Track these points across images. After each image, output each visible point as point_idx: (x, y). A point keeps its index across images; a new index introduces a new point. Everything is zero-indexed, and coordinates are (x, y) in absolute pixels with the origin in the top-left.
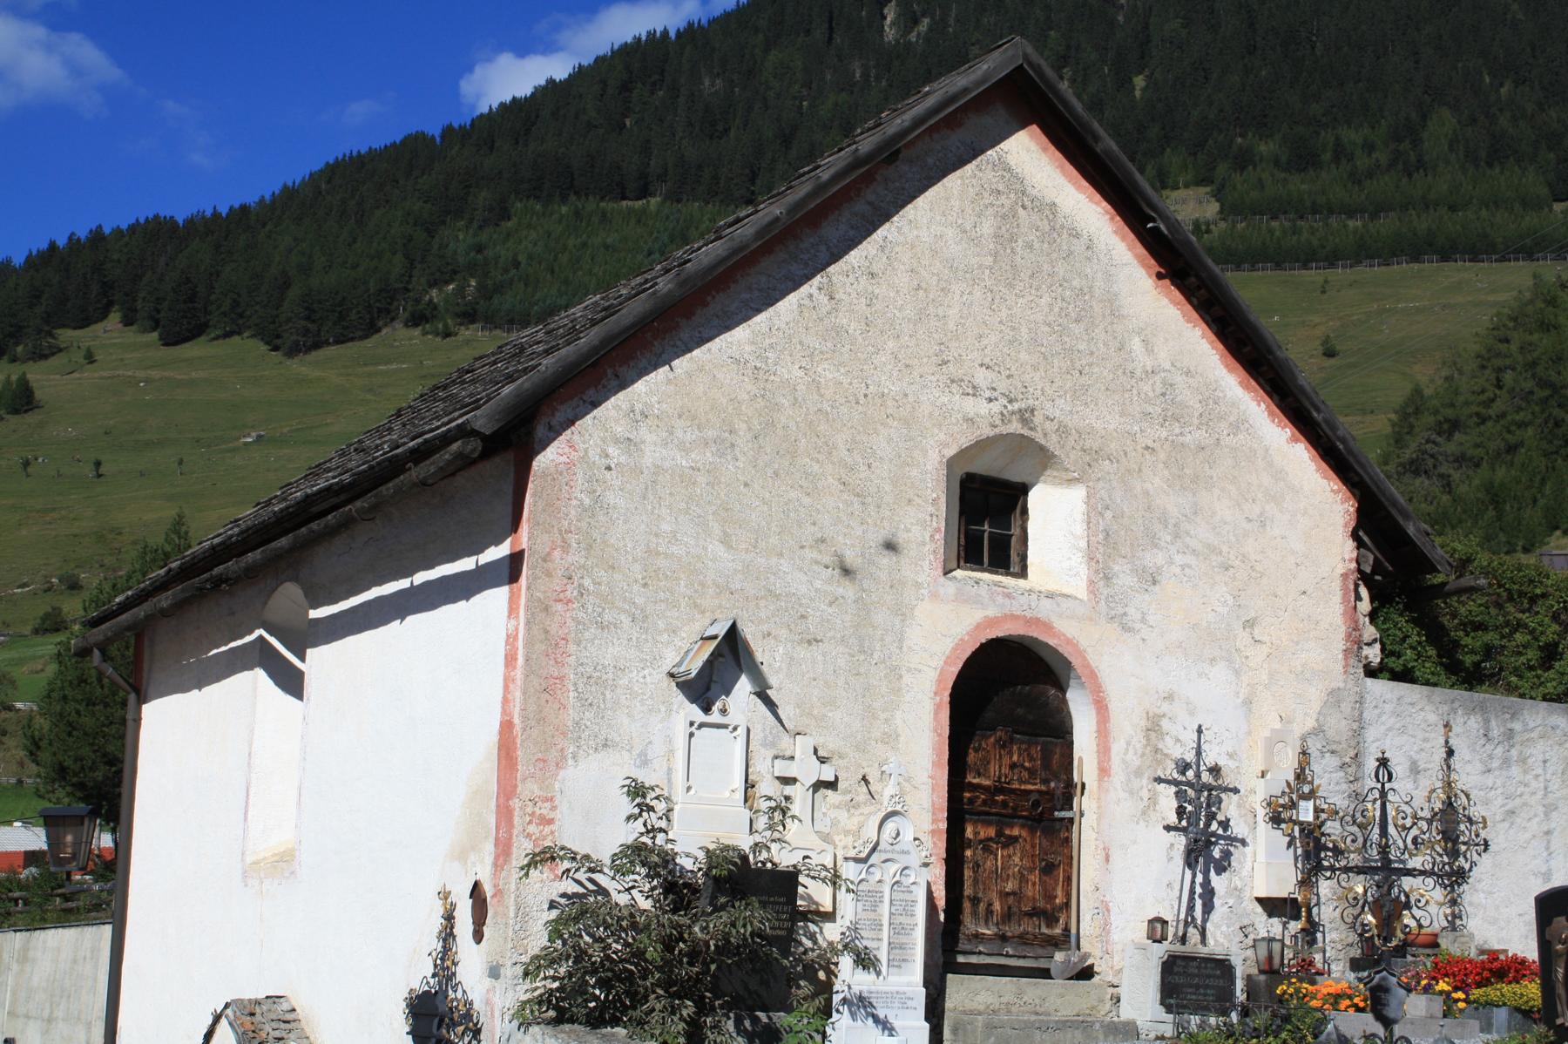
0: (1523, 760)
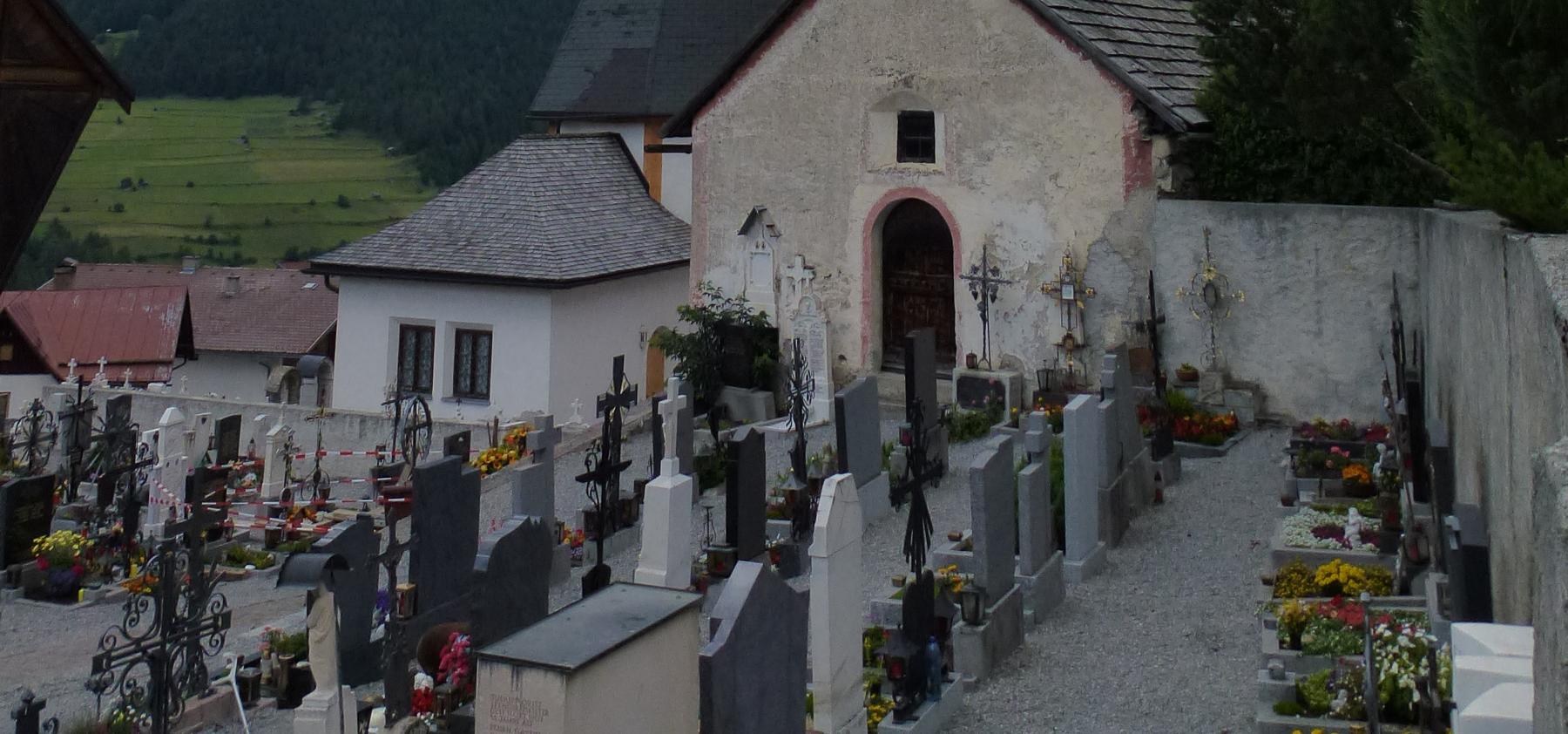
0: (1295, 250)
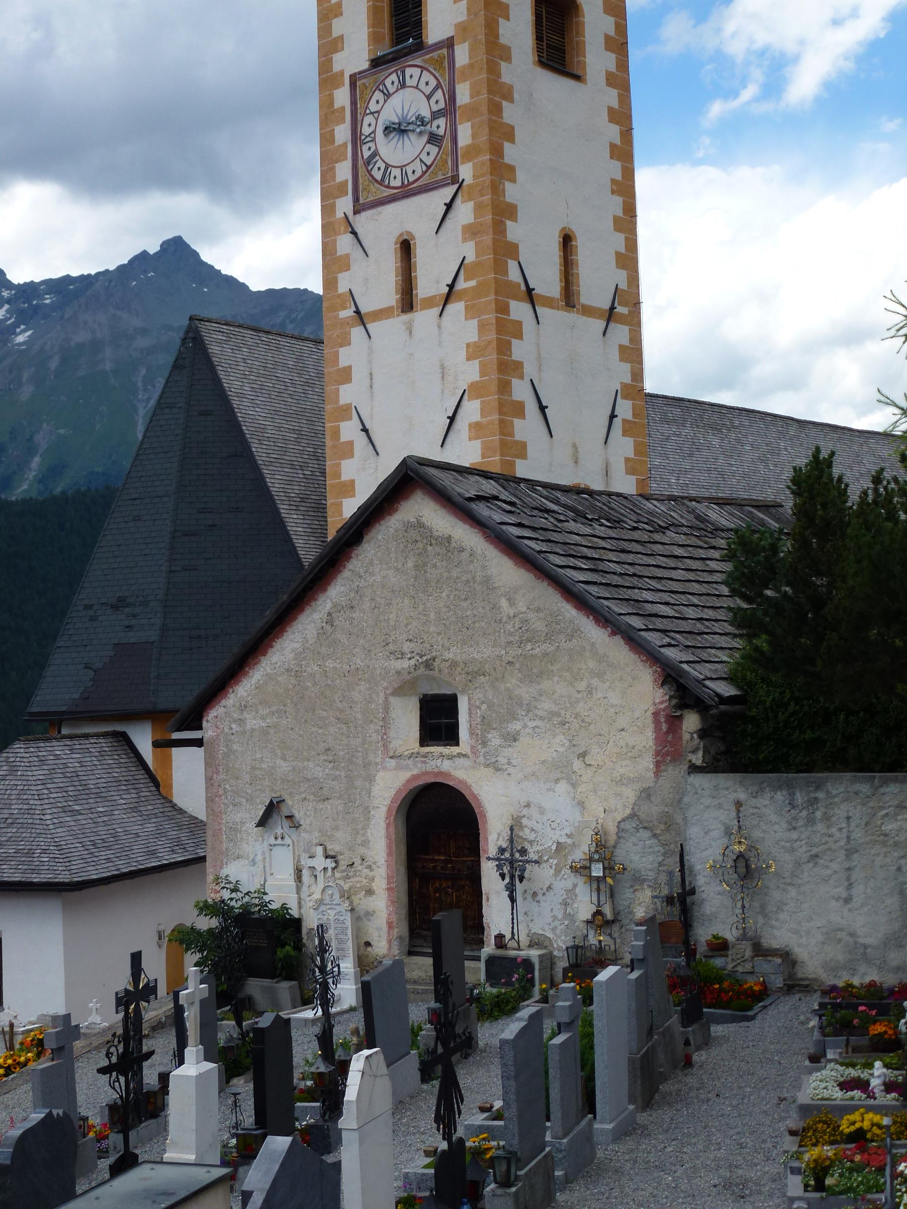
0: (827, 818)
